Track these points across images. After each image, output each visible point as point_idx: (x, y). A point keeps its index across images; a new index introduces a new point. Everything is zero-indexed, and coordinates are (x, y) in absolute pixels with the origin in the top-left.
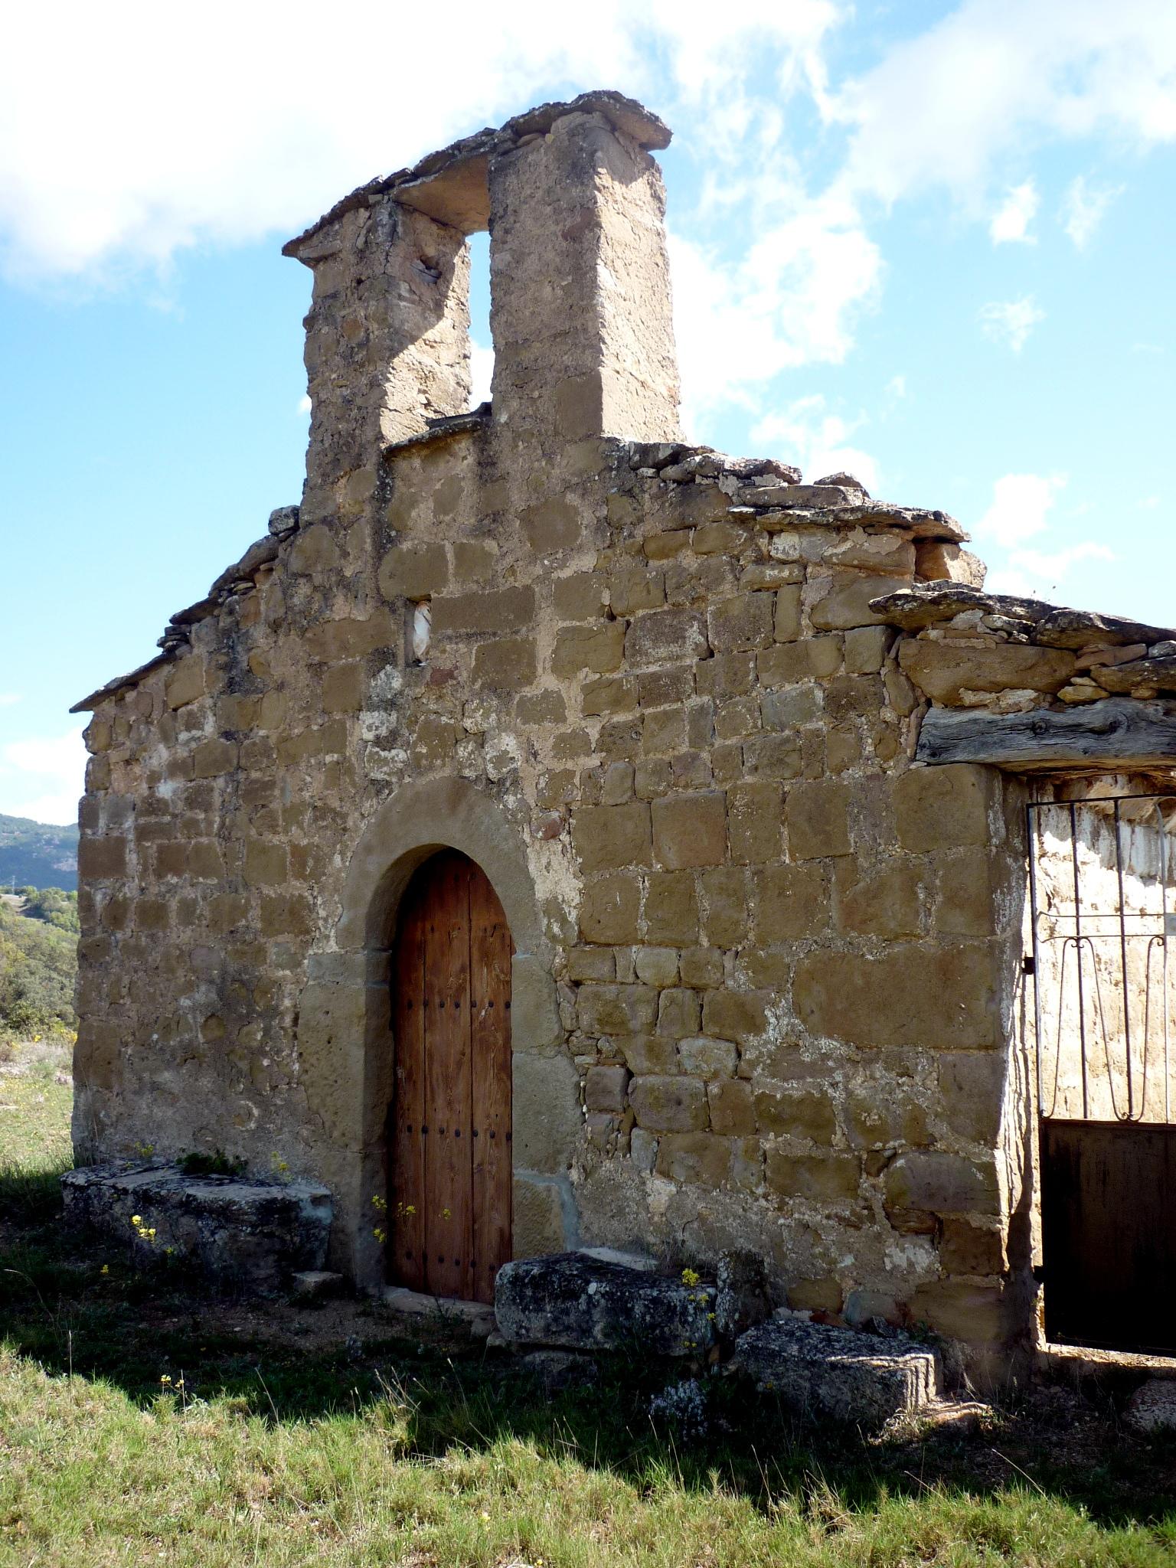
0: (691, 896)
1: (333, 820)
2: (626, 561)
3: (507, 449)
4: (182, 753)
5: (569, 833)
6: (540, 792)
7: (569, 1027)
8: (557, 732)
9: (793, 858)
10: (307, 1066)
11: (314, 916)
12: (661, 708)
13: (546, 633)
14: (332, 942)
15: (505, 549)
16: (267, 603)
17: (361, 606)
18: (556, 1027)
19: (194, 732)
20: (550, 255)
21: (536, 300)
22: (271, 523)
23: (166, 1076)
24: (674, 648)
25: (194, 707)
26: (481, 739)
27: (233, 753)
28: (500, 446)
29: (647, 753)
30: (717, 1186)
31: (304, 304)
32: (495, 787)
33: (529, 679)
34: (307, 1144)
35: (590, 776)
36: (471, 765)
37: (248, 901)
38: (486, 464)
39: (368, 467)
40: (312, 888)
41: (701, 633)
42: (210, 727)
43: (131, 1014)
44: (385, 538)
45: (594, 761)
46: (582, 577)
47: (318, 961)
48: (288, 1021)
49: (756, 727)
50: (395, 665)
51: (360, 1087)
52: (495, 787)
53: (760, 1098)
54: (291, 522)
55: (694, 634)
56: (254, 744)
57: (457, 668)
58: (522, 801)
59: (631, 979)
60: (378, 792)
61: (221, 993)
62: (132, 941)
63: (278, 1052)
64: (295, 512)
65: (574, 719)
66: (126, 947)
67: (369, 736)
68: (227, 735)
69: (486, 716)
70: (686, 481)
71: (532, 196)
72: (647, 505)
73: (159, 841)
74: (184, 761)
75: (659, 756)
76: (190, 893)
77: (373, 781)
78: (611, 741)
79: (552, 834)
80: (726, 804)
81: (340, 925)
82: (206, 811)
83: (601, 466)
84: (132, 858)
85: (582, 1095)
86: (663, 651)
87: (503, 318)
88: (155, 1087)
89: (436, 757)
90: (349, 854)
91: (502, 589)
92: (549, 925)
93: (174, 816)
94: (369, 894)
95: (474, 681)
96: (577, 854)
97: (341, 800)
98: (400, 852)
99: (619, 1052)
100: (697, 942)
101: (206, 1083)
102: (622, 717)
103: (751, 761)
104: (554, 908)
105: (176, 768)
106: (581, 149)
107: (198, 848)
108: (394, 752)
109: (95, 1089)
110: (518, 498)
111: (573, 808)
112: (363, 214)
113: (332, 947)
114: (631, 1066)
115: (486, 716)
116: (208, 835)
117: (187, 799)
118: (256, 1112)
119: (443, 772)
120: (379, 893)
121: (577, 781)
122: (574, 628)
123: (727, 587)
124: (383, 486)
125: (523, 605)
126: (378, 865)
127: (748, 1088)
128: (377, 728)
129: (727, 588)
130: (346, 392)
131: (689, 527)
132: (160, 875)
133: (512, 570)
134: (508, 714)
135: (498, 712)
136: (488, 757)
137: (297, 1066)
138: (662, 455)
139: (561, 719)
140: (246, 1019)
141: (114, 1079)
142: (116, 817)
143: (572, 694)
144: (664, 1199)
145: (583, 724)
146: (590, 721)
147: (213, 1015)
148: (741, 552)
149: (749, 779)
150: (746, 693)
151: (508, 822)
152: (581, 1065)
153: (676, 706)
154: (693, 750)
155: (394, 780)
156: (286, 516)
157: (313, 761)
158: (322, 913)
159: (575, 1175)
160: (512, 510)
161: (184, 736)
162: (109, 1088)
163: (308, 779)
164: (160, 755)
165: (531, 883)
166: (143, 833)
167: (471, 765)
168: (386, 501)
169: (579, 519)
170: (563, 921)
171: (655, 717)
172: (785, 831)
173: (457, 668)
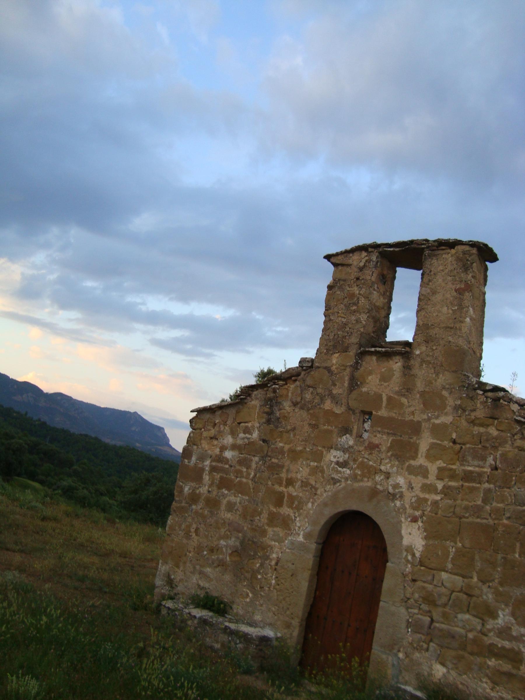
0: (473, 559)
1: (311, 488)
2: (464, 423)
3: (417, 365)
4: (239, 442)
5: (422, 522)
6: (412, 503)
7: (408, 596)
8: (424, 482)
9: (520, 556)
10: (279, 583)
11: (294, 524)
12: (471, 485)
13: (425, 442)
14: (301, 536)
15: (410, 404)
16: (292, 393)
17: (339, 407)
18: (402, 595)
19: (247, 435)
20: (448, 296)
21: (439, 312)
22: (300, 362)
23: (208, 570)
24: (481, 463)
25: (249, 425)
26: (388, 476)
27: (265, 449)
28: (415, 363)
29: (462, 500)
30: (465, 674)
31: (329, 280)
32: (393, 497)
33: (414, 458)
34: (274, 614)
35: (435, 503)
36: (381, 484)
37: (262, 510)
38: (407, 368)
39: (351, 353)
40: (295, 513)
41: (494, 460)
42: (255, 435)
43: (195, 540)
44: (354, 383)
45: (438, 498)
46: (444, 426)
47: (292, 543)
48: (273, 563)
49: (512, 502)
50: (351, 435)
51: (304, 597)
52: (393, 497)
53: (491, 645)
54: (310, 365)
55: (490, 460)
56: (277, 448)
57: (381, 444)
58: (403, 505)
59: (440, 585)
60: (335, 484)
61: (242, 543)
62: (201, 511)
63: (266, 574)
64: (312, 360)
65: (432, 478)
66: (196, 512)
67: (335, 460)
68: (264, 441)
69: (392, 466)
70: (496, 400)
71: (443, 271)
72: (478, 405)
73: (221, 475)
74: (240, 445)
75: (467, 503)
76: (232, 499)
77: (333, 479)
78: (447, 492)
79: (415, 520)
80: (494, 528)
81: (305, 531)
82: (247, 468)
83: (460, 384)
84: (206, 478)
85: (408, 624)
86: (476, 463)
87: (423, 313)
88: (201, 573)
89: (365, 477)
90: (316, 504)
91: (407, 419)
92: (406, 556)
93: (231, 466)
94: (323, 522)
95: (388, 452)
96: (424, 531)
97: (316, 482)
98: (341, 509)
99: (430, 611)
100: (472, 578)
101: (228, 577)
102: (453, 484)
103: (508, 515)
104: (410, 549)
105: (234, 447)
106: (468, 260)
107: (240, 483)
108: (345, 469)
109: (171, 566)
110: (420, 386)
111: (425, 513)
112: (364, 254)
113: (301, 538)
114: (434, 618)
115: (392, 466)
116: (246, 478)
117: (238, 461)
118: (250, 595)
119: (367, 484)
120: (326, 523)
121: (429, 503)
122: (438, 444)
123: (507, 446)
124: (357, 363)
125: (416, 429)
126: (329, 512)
127: (485, 638)
128: (338, 458)
129: (508, 447)
130: (344, 320)
131: (496, 419)
132: (219, 488)
133: (413, 413)
134: (402, 469)
135: (398, 467)
136: (390, 483)
137: (274, 582)
138: (487, 388)
139: (425, 476)
140: (254, 557)
141: (181, 564)
142: (202, 458)
143: (433, 468)
144: (441, 674)
145: (436, 482)
146: (439, 482)
147: (236, 551)
148: (516, 434)
149: (505, 521)
150: (509, 488)
151: (395, 511)
152: (411, 613)
153: (478, 485)
154: (482, 504)
155: (343, 480)
156: (308, 361)
157: (304, 463)
158: (298, 524)
159: (401, 655)
160: (416, 389)
161: (242, 435)
162: (178, 567)
163: (301, 469)
164: (229, 440)
165: (402, 538)
166: (213, 469)
167: (381, 484)
168: (357, 369)
169: (447, 402)
170: (413, 555)
171: (469, 488)
172: (518, 545)
173: (381, 444)
